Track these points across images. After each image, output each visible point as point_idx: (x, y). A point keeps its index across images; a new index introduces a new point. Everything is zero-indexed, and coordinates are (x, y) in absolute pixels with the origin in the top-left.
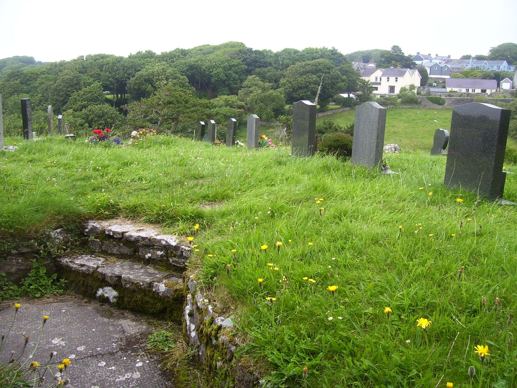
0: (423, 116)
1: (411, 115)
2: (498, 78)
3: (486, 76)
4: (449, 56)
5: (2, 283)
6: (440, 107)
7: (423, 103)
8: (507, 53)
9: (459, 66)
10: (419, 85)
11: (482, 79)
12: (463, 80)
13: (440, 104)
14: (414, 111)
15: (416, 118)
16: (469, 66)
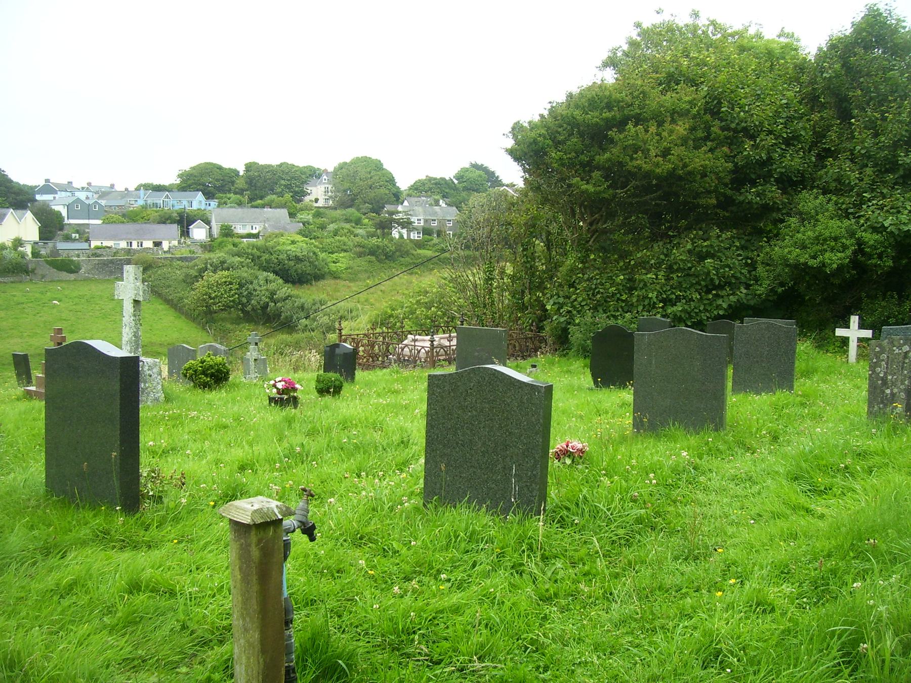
0: (37, 295)
1: (14, 296)
2: (185, 222)
3: (165, 219)
4: (112, 186)
5: (894, 681)
6: (72, 276)
7: (39, 272)
8: (207, 180)
9: (122, 203)
10: (37, 239)
11: (159, 223)
12: (121, 226)
13: (71, 271)
14: (21, 286)
15: (24, 299)
16: (141, 202)
